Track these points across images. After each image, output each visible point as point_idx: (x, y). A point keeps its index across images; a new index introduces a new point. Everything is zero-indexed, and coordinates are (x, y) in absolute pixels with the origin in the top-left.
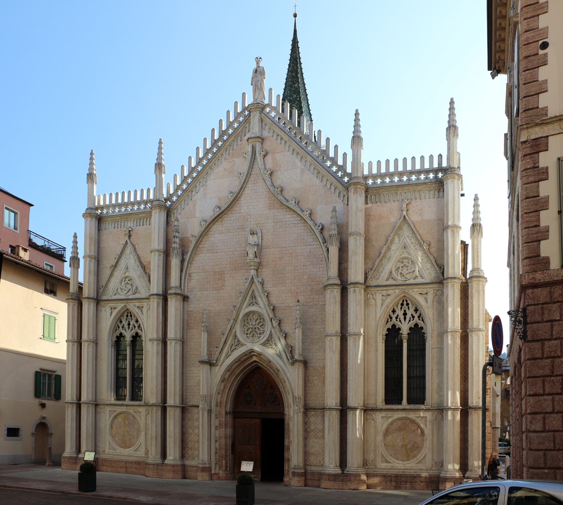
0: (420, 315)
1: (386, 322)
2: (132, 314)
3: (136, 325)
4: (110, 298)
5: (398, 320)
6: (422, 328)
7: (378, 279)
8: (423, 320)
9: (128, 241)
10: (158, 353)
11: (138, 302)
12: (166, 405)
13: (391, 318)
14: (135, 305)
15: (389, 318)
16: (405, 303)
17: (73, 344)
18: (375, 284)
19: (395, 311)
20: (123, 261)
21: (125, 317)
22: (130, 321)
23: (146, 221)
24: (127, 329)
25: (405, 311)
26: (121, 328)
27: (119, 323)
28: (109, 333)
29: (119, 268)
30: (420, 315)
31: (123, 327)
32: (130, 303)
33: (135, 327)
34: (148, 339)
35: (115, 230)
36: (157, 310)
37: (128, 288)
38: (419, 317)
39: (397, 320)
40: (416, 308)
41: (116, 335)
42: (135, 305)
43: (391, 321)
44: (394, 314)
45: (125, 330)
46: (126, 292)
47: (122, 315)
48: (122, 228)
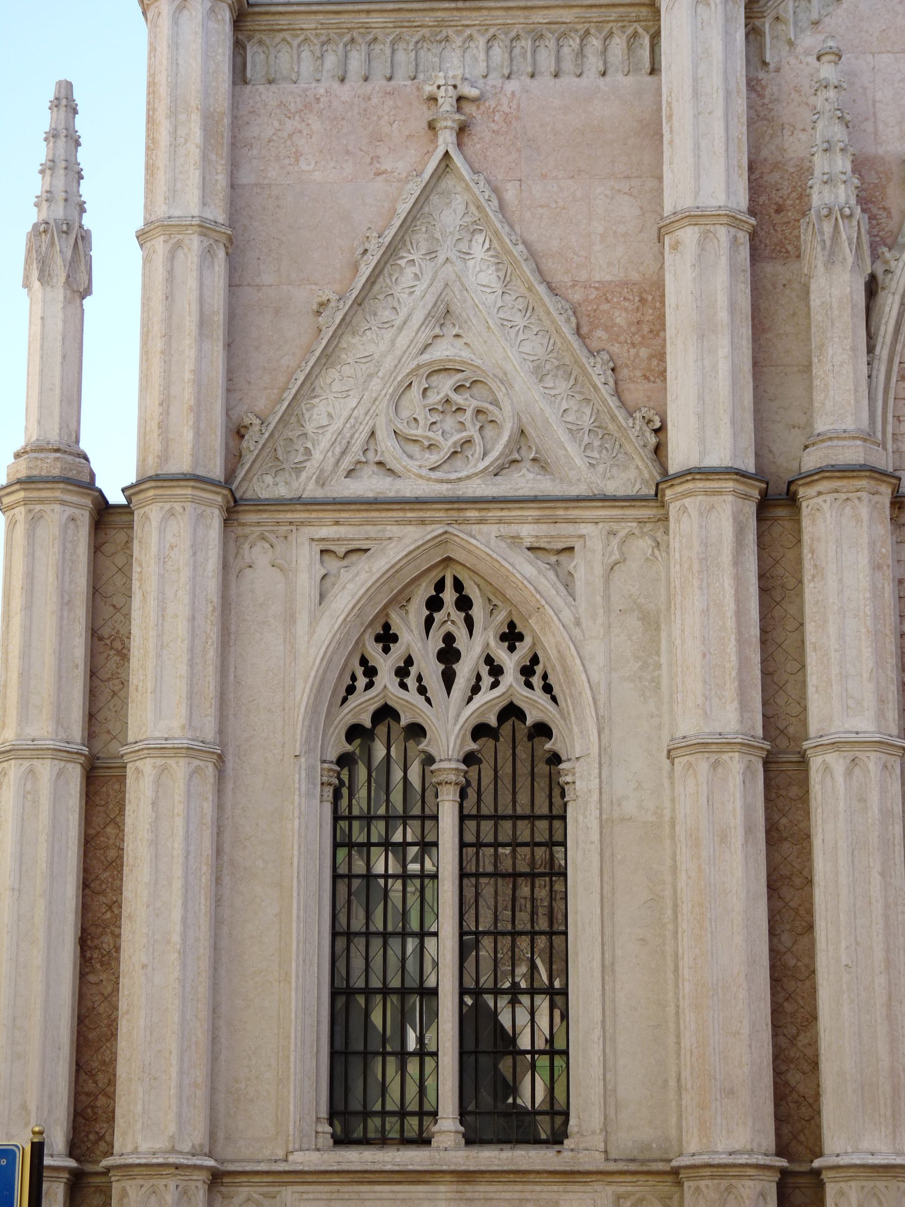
0: (535, 660)
1: (343, 693)
2: (472, 591)
3: (510, 662)
4: (311, 491)
5: (411, 681)
6: (543, 730)
7: (298, 470)
8: (548, 689)
9: (457, 158)
10: (749, 830)
11: (537, 521)
12: (817, 1163)
13: (371, 672)
14: (515, 540)
15: (359, 671)
16: (449, 596)
17: (60, 774)
18: (282, 491)
19: (395, 638)
20: (410, 272)
21: (417, 611)
22: (460, 632)
23: (580, 54)
24: (434, 683)
25: (449, 638)
26: (386, 678)
27: (374, 651)
28: (314, 709)
29: (386, 315)
30: (535, 660)
31: (402, 672)
32: (481, 521)
33: (496, 671)
34: (858, 754)
35: (345, 92)
36: (737, 562)
37: (437, 436)
38: (527, 671)
39: (403, 686)
40: (512, 625)
41: (351, 720)
42: (515, 540)
43: (369, 686)
44: (386, 650)
45: (422, 690)
46: (434, 458)
47: (401, 600)
48: (400, 81)
